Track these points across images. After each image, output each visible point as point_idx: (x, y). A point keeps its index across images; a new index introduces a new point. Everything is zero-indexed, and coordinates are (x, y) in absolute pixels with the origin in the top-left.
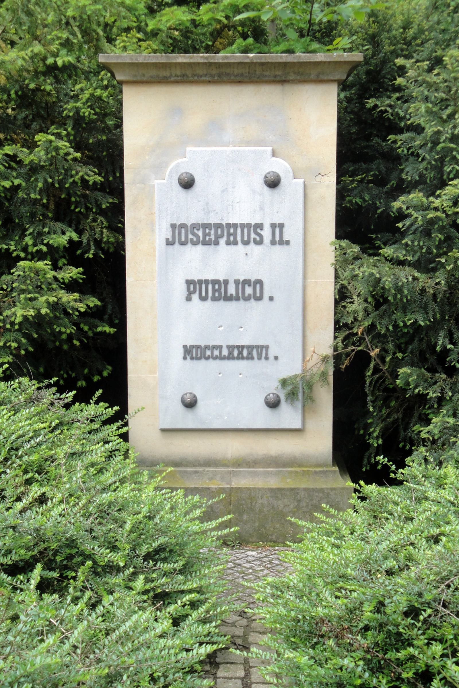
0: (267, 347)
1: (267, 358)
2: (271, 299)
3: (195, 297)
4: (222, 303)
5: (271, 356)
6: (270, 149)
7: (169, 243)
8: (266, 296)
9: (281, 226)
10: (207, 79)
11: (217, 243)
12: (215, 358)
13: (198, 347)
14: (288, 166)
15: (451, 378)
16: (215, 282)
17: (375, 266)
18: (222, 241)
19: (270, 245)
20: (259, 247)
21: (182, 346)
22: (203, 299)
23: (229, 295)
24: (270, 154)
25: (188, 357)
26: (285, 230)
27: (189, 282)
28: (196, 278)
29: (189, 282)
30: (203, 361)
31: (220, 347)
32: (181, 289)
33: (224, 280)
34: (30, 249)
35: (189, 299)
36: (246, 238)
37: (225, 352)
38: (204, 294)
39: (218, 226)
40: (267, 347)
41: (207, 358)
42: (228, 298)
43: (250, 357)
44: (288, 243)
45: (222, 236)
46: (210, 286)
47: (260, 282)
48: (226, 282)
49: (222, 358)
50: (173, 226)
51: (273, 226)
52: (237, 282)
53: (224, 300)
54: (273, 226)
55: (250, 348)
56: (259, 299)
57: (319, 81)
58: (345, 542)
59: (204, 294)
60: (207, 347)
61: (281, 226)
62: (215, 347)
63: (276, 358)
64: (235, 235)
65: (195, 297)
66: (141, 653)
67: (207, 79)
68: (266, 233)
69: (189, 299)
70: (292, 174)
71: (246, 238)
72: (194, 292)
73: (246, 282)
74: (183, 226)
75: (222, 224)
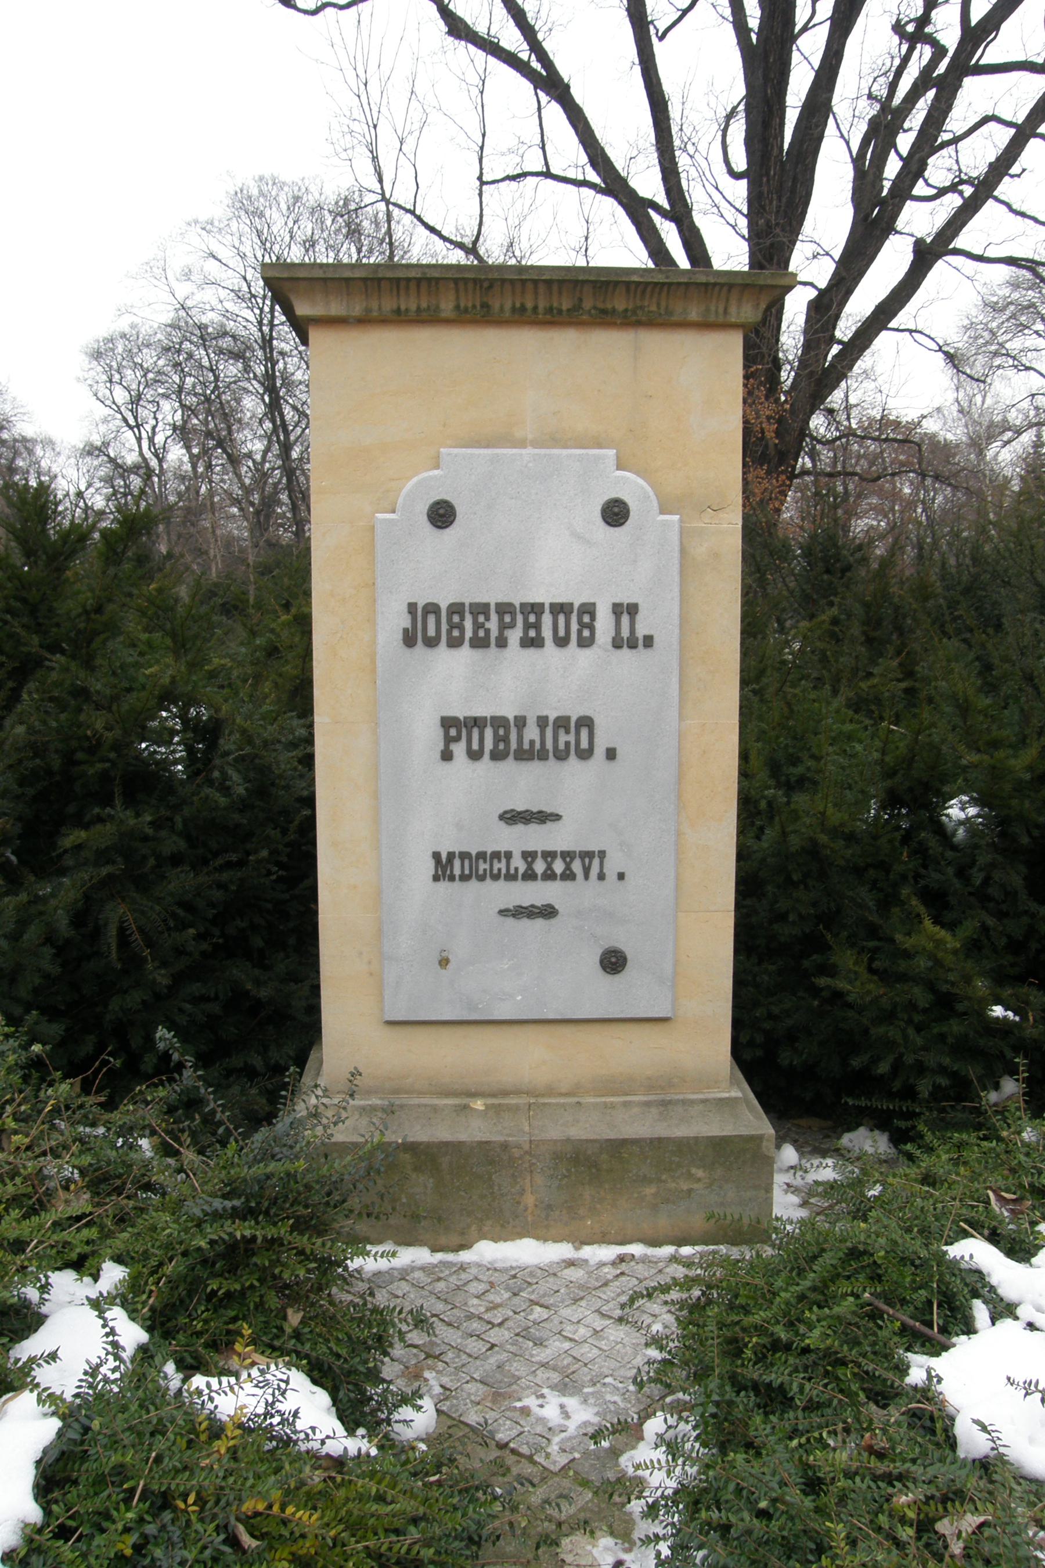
0: (602, 854)
1: (601, 877)
2: (611, 754)
3: (459, 749)
5: (612, 868)
6: (612, 452)
7: (409, 639)
8: (600, 751)
9: (633, 610)
10: (512, 1101)
11: (502, 643)
12: (496, 877)
13: (464, 856)
14: (649, 489)
16: (499, 722)
18: (514, 636)
19: (610, 647)
20: (587, 652)
21: (430, 853)
22: (474, 755)
23: (526, 746)
24: (612, 462)
26: (639, 617)
27: (447, 723)
28: (460, 713)
29: (447, 723)
30: (474, 883)
31: (509, 855)
32: (431, 736)
33: (516, 717)
36: (562, 633)
37: (519, 864)
38: (475, 746)
39: (504, 609)
40: (602, 854)
41: (481, 878)
42: (524, 755)
43: (568, 876)
45: (512, 625)
46: (489, 733)
47: (586, 723)
49: (511, 877)
50: (412, 608)
51: (617, 610)
52: (542, 722)
53: (516, 759)
54: (617, 610)
55: (567, 856)
56: (585, 755)
59: (475, 746)
60: (482, 855)
61: (633, 610)
62: (496, 855)
63: (621, 876)
64: (537, 626)
65: (459, 749)
66: (75, 1493)
67: (512, 1101)
69: (447, 756)
70: (655, 504)
71: (562, 633)
72: (457, 739)
74: (432, 609)
75: (511, 605)
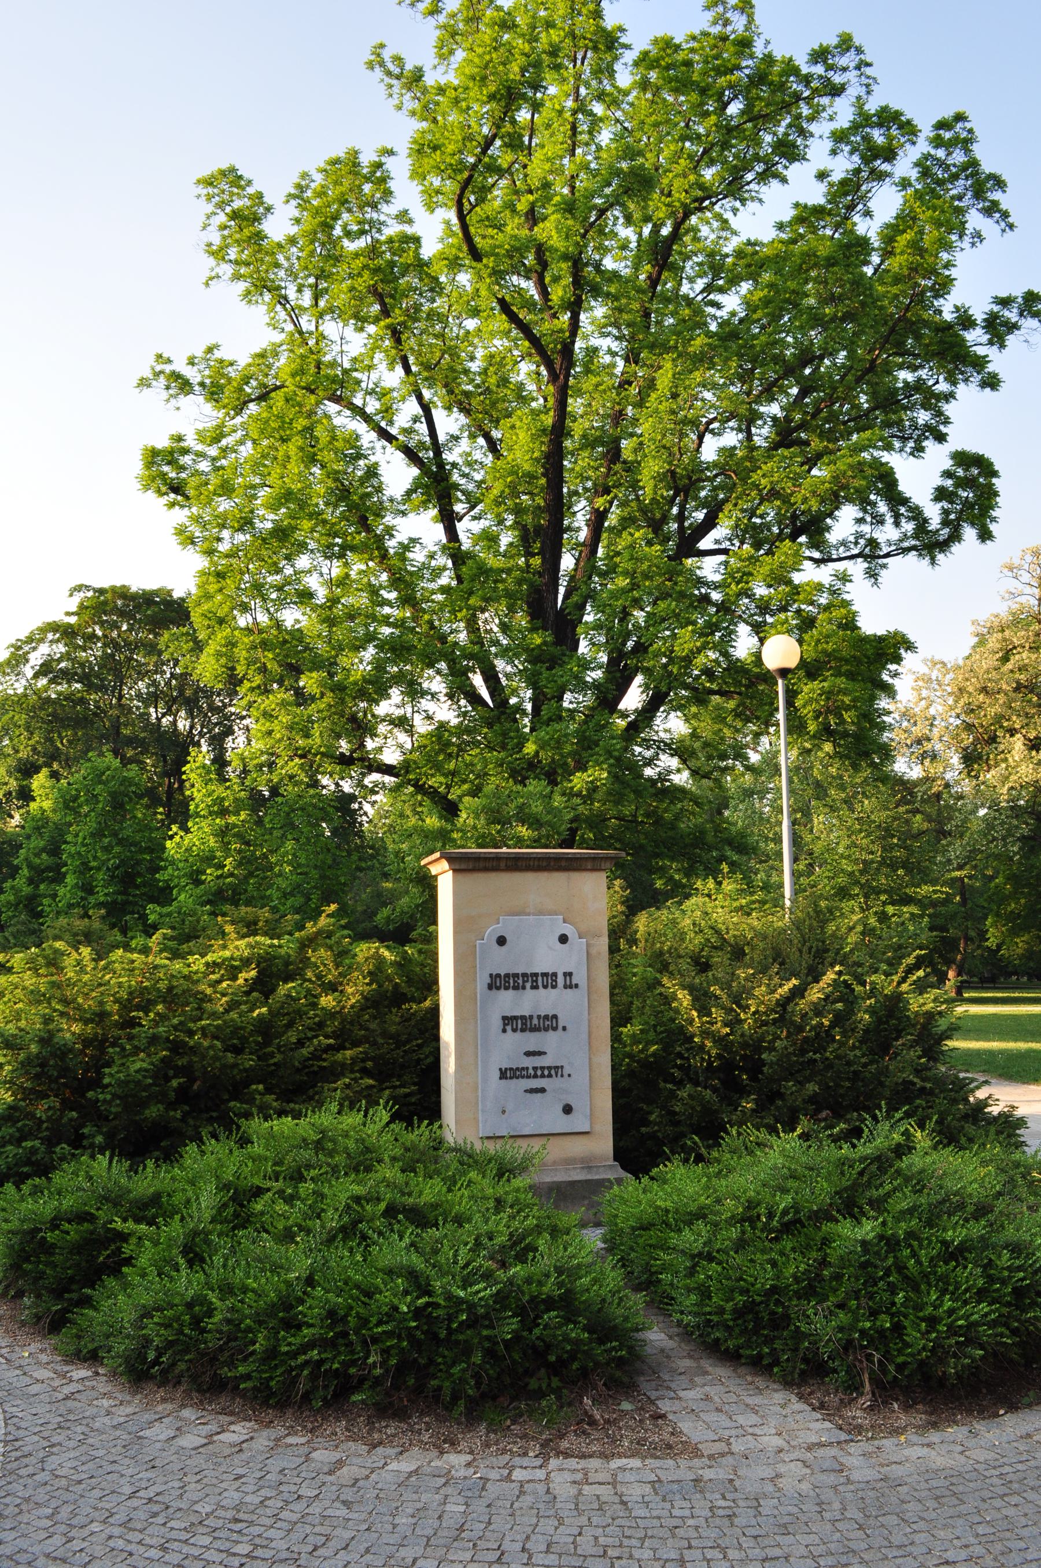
2: (564, 1028)
4: (527, 1034)
5: (565, 1074)
9: (570, 974)
11: (524, 988)
15: (919, 379)
16: (523, 1018)
17: (769, 457)
18: (528, 985)
22: (514, 1030)
25: (509, 1028)
27: (504, 1018)
28: (509, 1014)
29: (504, 1018)
32: (497, 1023)
34: (431, 79)
35: (504, 1031)
39: (525, 975)
43: (550, 1076)
44: (577, 986)
47: (555, 1017)
48: (531, 1017)
49: (528, 1077)
51: (565, 974)
52: (539, 1017)
54: (565, 974)
56: (555, 1029)
57: (594, 870)
58: (622, 1244)
68: (560, 980)
69: (504, 1031)
73: (546, 1017)
74: (498, 976)
